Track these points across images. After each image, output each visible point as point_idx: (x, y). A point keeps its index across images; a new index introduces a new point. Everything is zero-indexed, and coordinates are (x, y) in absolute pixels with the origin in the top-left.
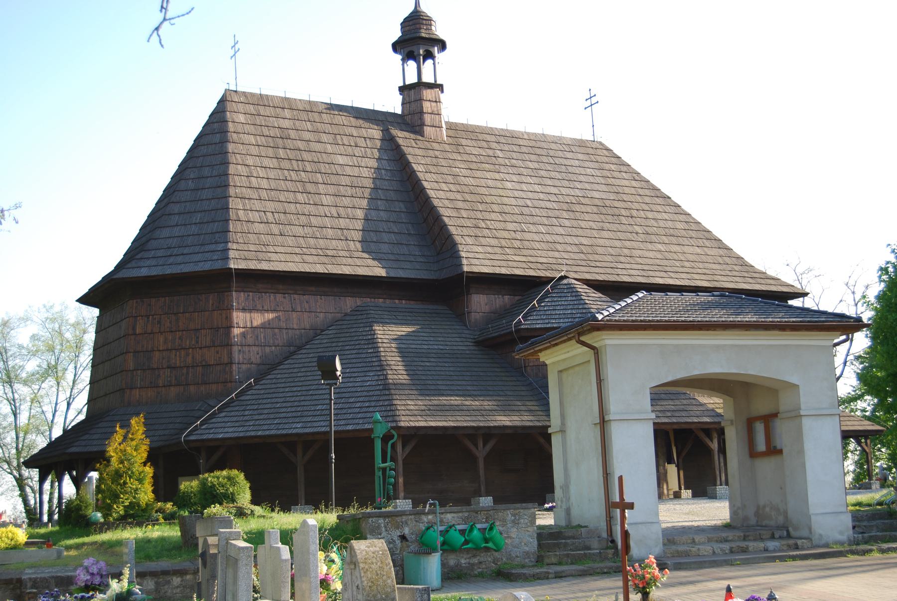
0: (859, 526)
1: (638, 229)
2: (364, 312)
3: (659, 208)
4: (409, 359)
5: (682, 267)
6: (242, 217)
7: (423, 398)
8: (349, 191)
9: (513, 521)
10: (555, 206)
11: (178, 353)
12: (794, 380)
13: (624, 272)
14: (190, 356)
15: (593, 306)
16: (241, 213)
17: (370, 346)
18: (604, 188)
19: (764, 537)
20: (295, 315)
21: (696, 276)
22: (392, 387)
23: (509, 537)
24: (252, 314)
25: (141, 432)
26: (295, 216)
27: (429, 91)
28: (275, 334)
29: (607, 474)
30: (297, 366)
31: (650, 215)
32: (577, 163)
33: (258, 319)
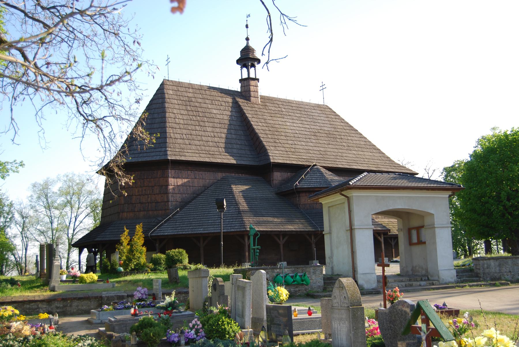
0: (458, 275)
1: (344, 144)
2: (227, 179)
3: (353, 135)
4: (248, 200)
5: (364, 161)
6: (173, 136)
7: (256, 218)
8: (219, 126)
9: (313, 272)
10: (308, 133)
11: (144, 197)
12: (432, 212)
13: (340, 163)
14: (150, 198)
15: (329, 178)
16: (172, 134)
17: (231, 194)
18: (329, 126)
19: (418, 280)
20: (196, 180)
21: (370, 165)
22: (242, 213)
23: (311, 279)
24: (177, 179)
25: (140, 231)
26: (196, 136)
27: (253, 81)
28: (187, 189)
29: (353, 252)
30: (198, 203)
31: (349, 138)
32: (317, 114)
33: (180, 182)
